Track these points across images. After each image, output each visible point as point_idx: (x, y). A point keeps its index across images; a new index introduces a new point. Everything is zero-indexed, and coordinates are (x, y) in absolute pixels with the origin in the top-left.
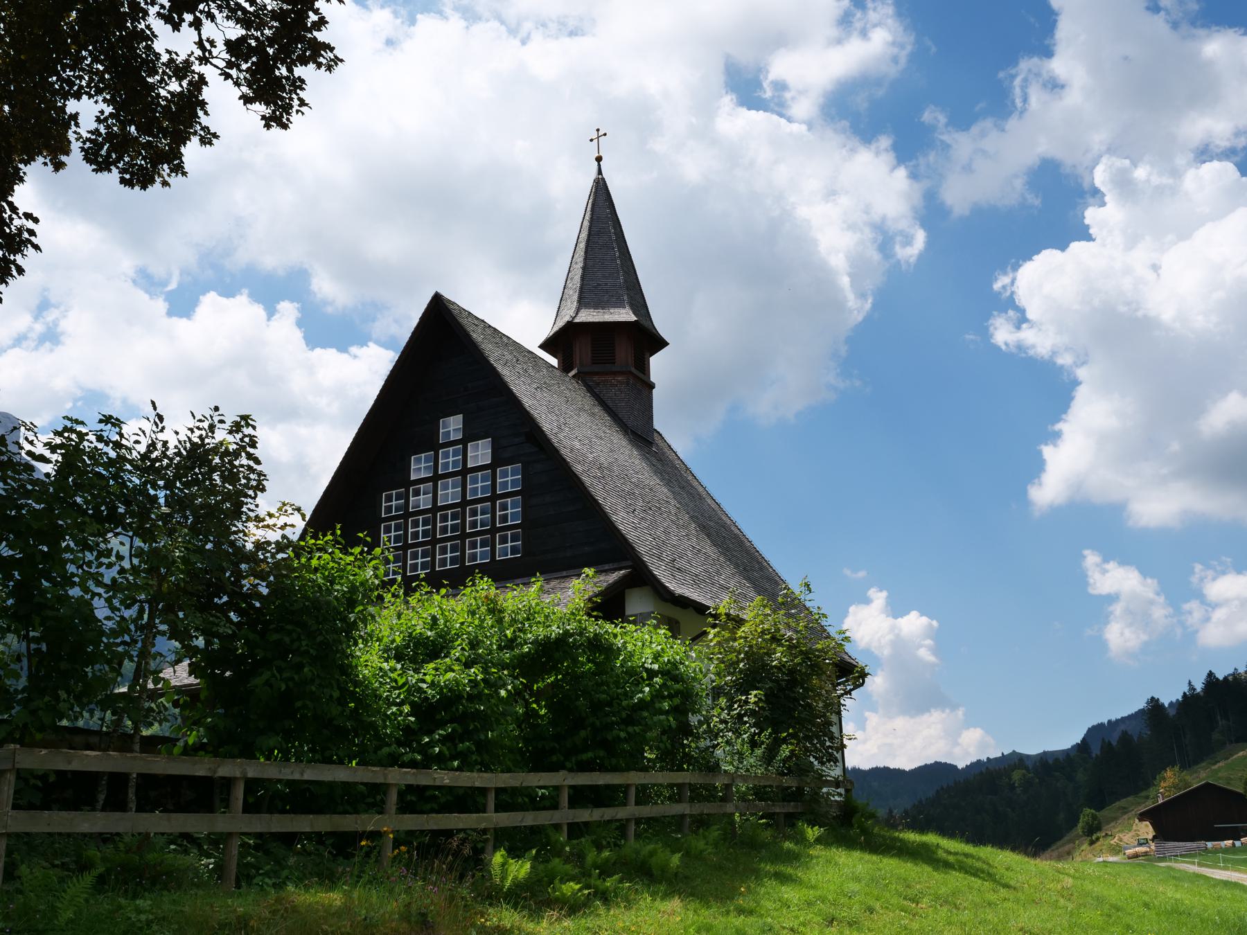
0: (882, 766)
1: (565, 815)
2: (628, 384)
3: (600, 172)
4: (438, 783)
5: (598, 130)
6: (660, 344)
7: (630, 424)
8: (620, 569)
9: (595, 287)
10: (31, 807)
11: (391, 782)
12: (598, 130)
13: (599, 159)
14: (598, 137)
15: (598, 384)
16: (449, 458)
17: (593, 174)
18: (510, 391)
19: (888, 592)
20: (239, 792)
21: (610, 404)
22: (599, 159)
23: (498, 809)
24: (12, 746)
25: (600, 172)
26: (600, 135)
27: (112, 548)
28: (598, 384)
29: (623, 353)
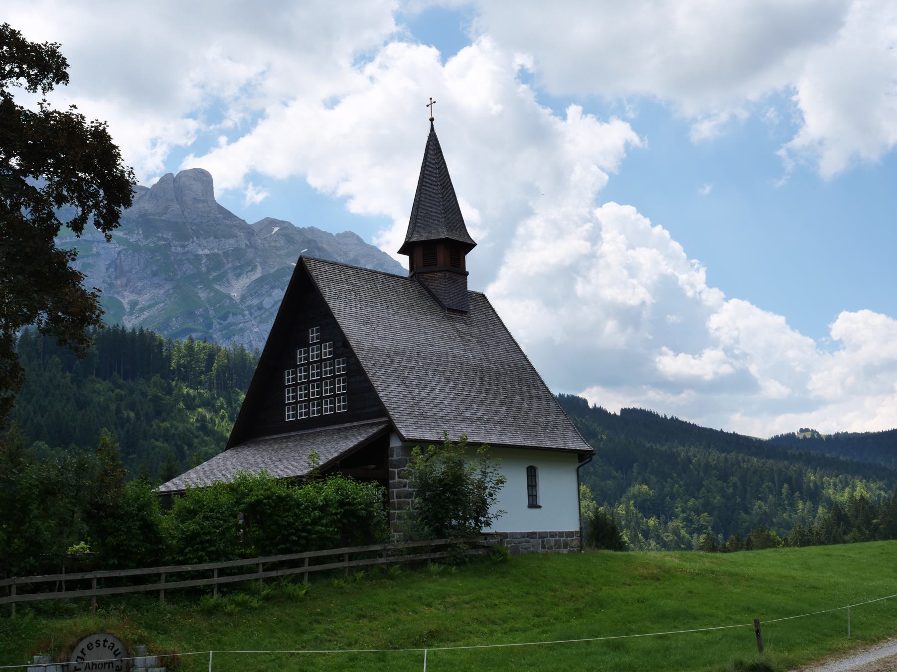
0: (833, 433)
1: (261, 574)
2: (444, 278)
3: (432, 129)
4: (185, 570)
5: (431, 99)
6: (471, 245)
7: (446, 304)
8: (372, 425)
9: (425, 215)
10: (19, 594)
11: (162, 572)
12: (431, 99)
13: (432, 120)
14: (431, 104)
15: (427, 280)
16: (316, 354)
17: (428, 132)
18: (334, 319)
19: (591, 409)
20: (95, 583)
21: (434, 291)
22: (432, 120)
23: (219, 576)
24: (13, 578)
25: (432, 129)
26: (432, 103)
27: (564, 117)
28: (427, 280)
29: (442, 257)
